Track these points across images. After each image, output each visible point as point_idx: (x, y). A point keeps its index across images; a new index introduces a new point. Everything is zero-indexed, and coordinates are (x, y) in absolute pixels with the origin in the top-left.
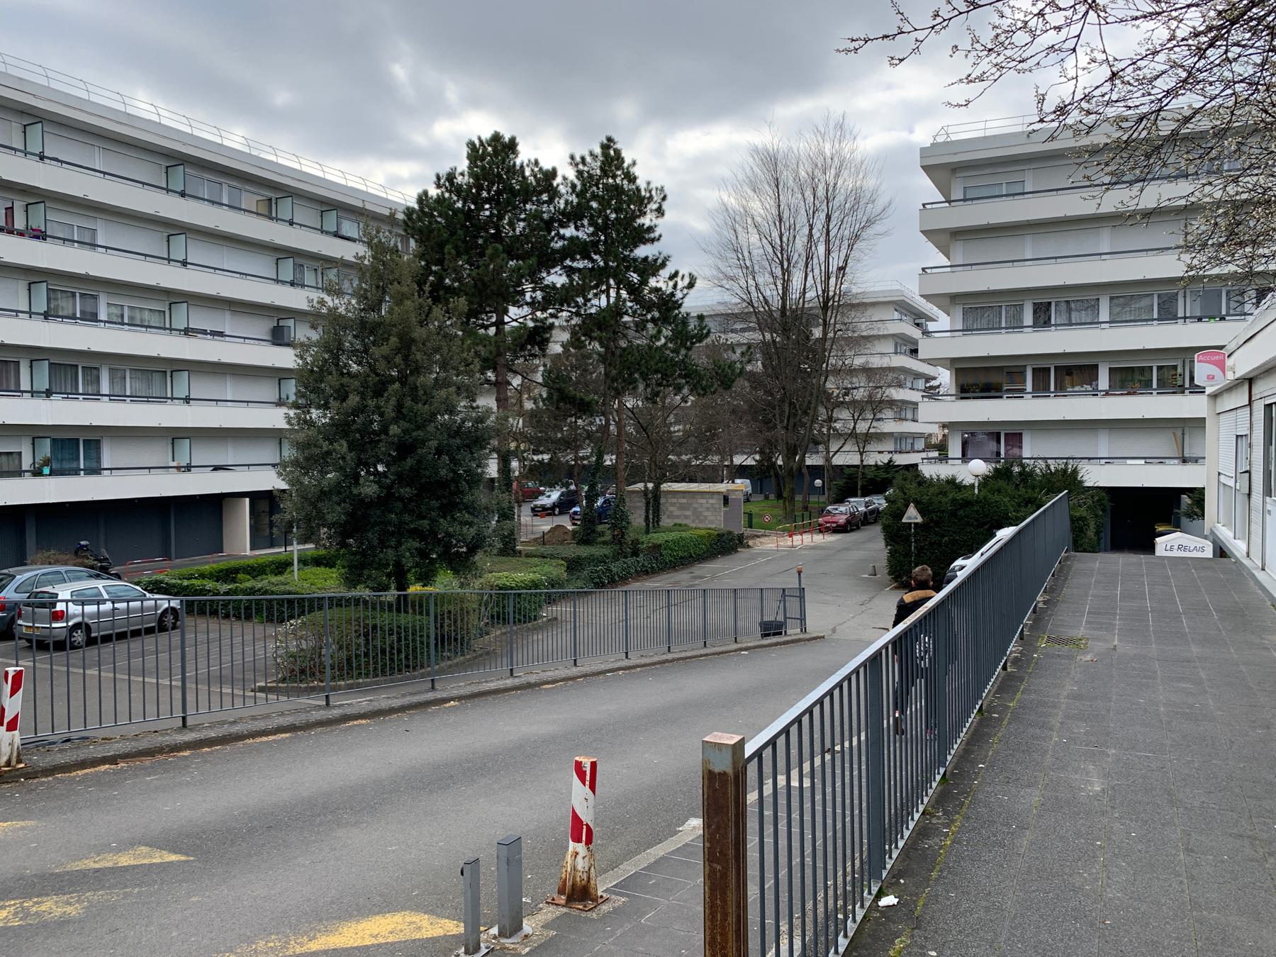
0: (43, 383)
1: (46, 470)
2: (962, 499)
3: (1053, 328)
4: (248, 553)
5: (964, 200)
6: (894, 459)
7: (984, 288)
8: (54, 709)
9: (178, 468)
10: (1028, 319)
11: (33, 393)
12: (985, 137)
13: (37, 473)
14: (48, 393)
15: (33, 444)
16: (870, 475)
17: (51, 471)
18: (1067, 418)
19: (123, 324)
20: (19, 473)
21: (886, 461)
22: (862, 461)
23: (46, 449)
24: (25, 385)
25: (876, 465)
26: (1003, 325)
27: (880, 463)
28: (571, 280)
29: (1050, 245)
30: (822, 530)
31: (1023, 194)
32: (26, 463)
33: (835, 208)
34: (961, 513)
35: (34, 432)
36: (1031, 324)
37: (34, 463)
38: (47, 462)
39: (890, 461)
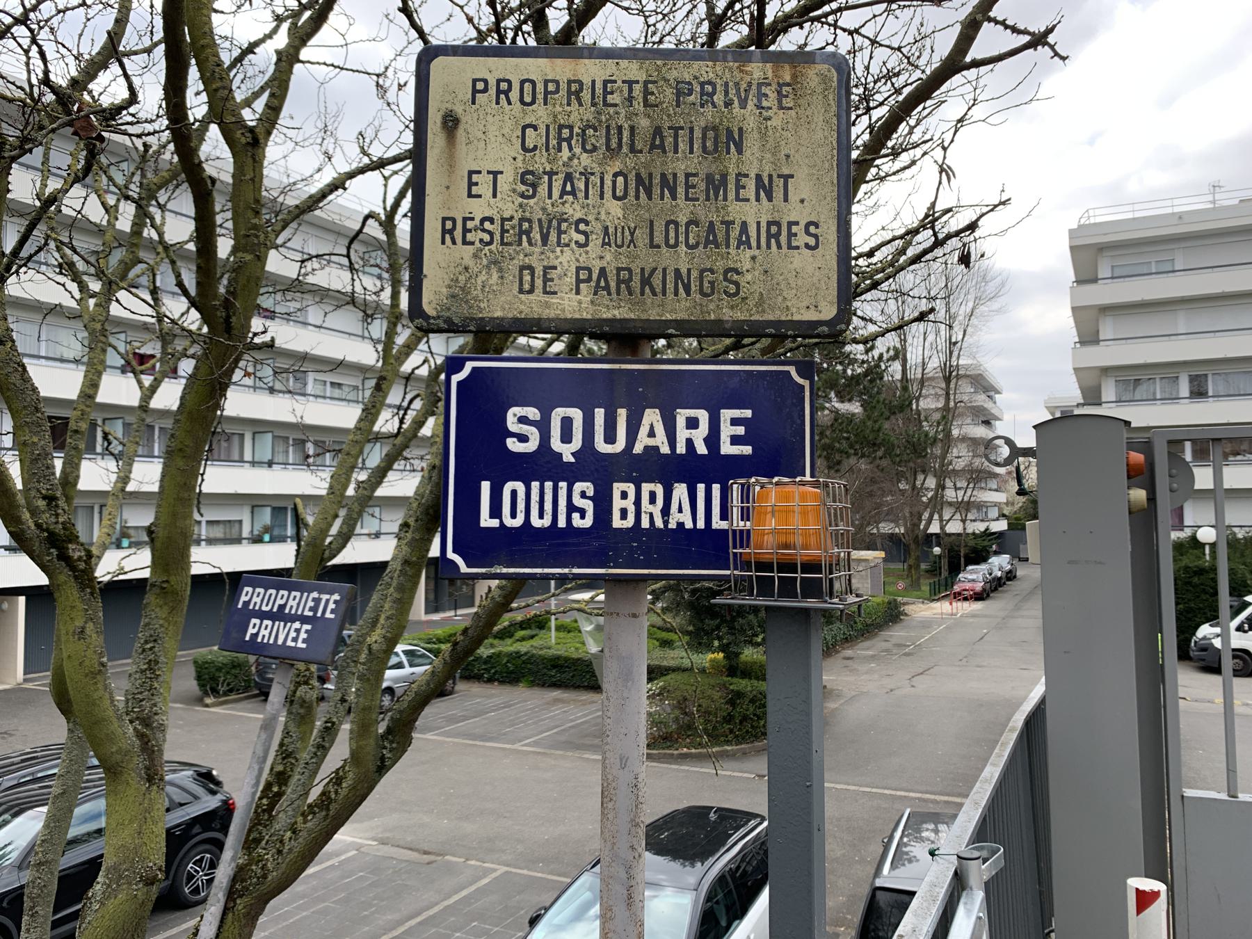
0: (265, 453)
1: (267, 538)
2: (1196, 566)
3: (1211, 399)
4: (424, 617)
5: (1112, 278)
6: (991, 527)
7: (1141, 361)
8: (1239, 749)
9: (369, 535)
10: (1184, 389)
11: (254, 463)
12: (1134, 219)
13: (257, 540)
14: (270, 464)
15: (252, 512)
16: (972, 543)
17: (271, 538)
18: (1235, 487)
19: (1155, 400)
20: (238, 540)
21: (983, 530)
22: (965, 529)
23: (266, 516)
24: (248, 456)
25: (974, 534)
26: (1158, 397)
27: (977, 532)
28: (193, 356)
29: (1204, 320)
30: (958, 596)
31: (1174, 271)
32: (246, 534)
33: (954, 288)
34: (1195, 580)
35: (255, 502)
36: (1188, 395)
37: (252, 531)
38: (267, 530)
39: (987, 529)
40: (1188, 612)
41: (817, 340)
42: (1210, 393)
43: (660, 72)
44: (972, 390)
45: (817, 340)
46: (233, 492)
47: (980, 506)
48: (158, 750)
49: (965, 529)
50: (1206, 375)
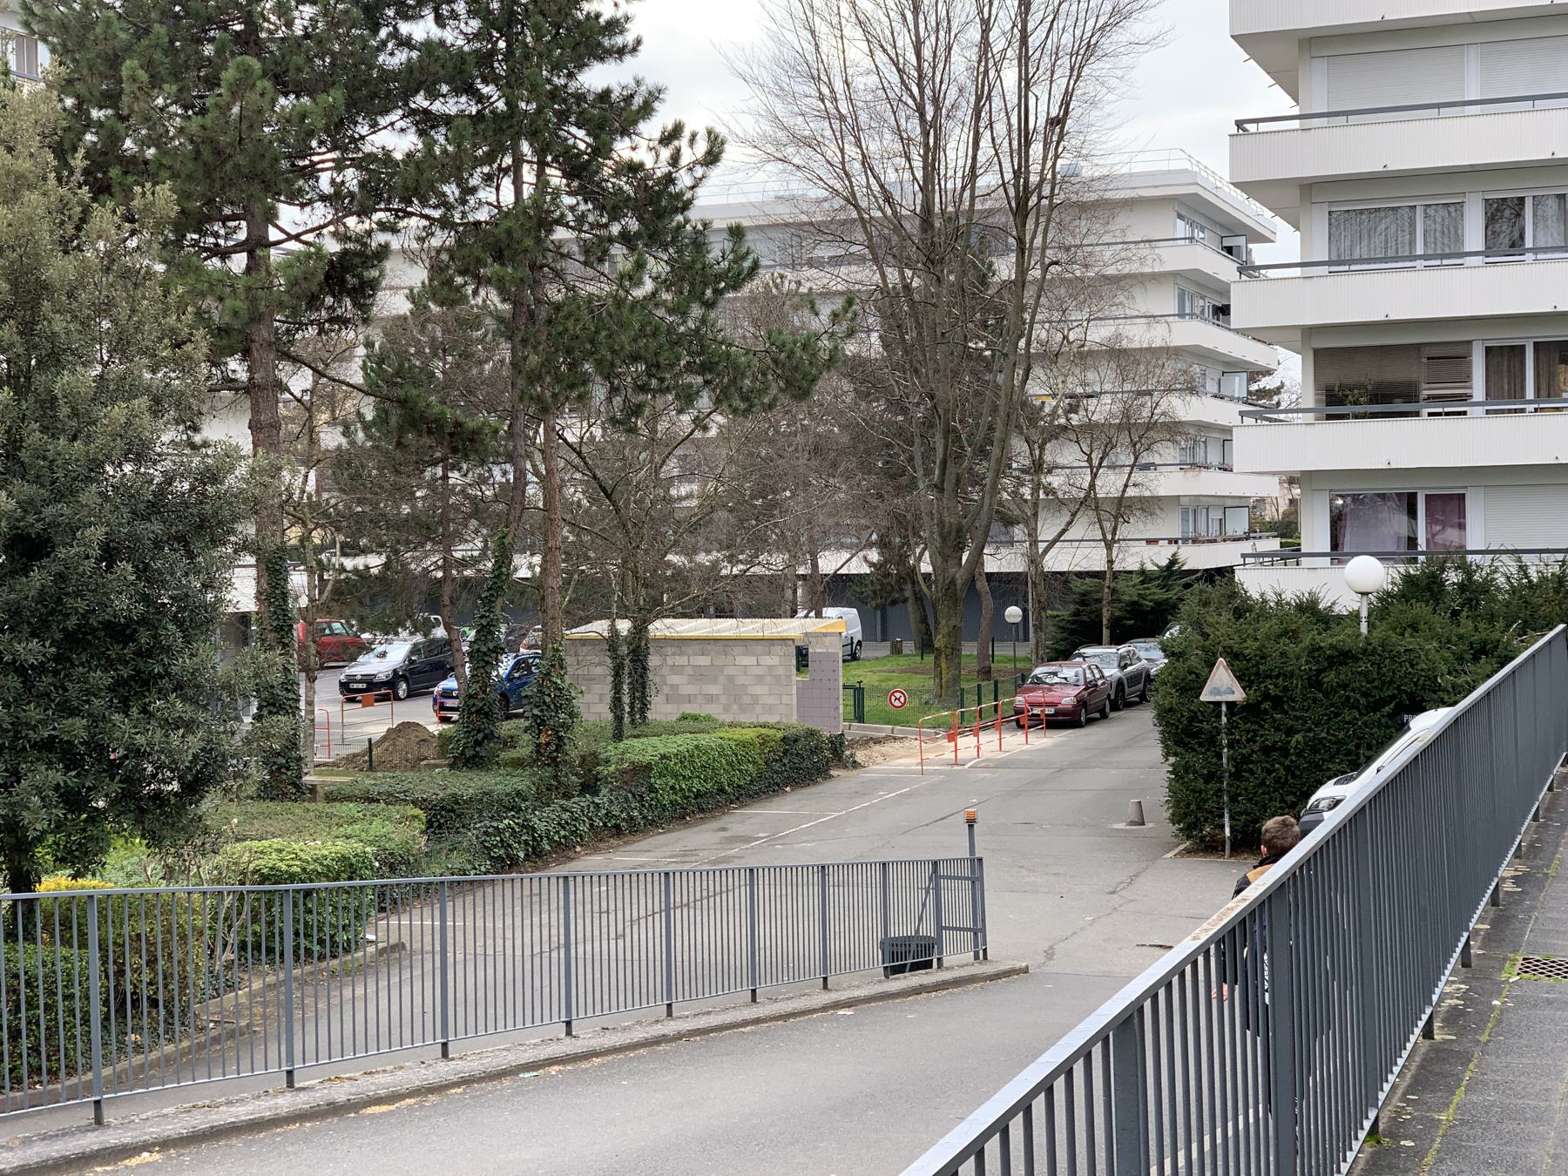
2: (1331, 647)
6: (1181, 557)
10: (1474, 234)
16: (1129, 593)
21: (1164, 562)
22: (1111, 562)
26: (1420, 251)
27: (1150, 567)
34: (1330, 677)
36: (1481, 248)
40: (1315, 751)
41: (931, 144)
42: (1529, 243)
43: (453, 226)
44: (369, 417)
45: (931, 144)
46: (1380, 317)
47: (1150, 506)
48: (261, 594)
49: (1111, 562)
50: (1522, 200)
